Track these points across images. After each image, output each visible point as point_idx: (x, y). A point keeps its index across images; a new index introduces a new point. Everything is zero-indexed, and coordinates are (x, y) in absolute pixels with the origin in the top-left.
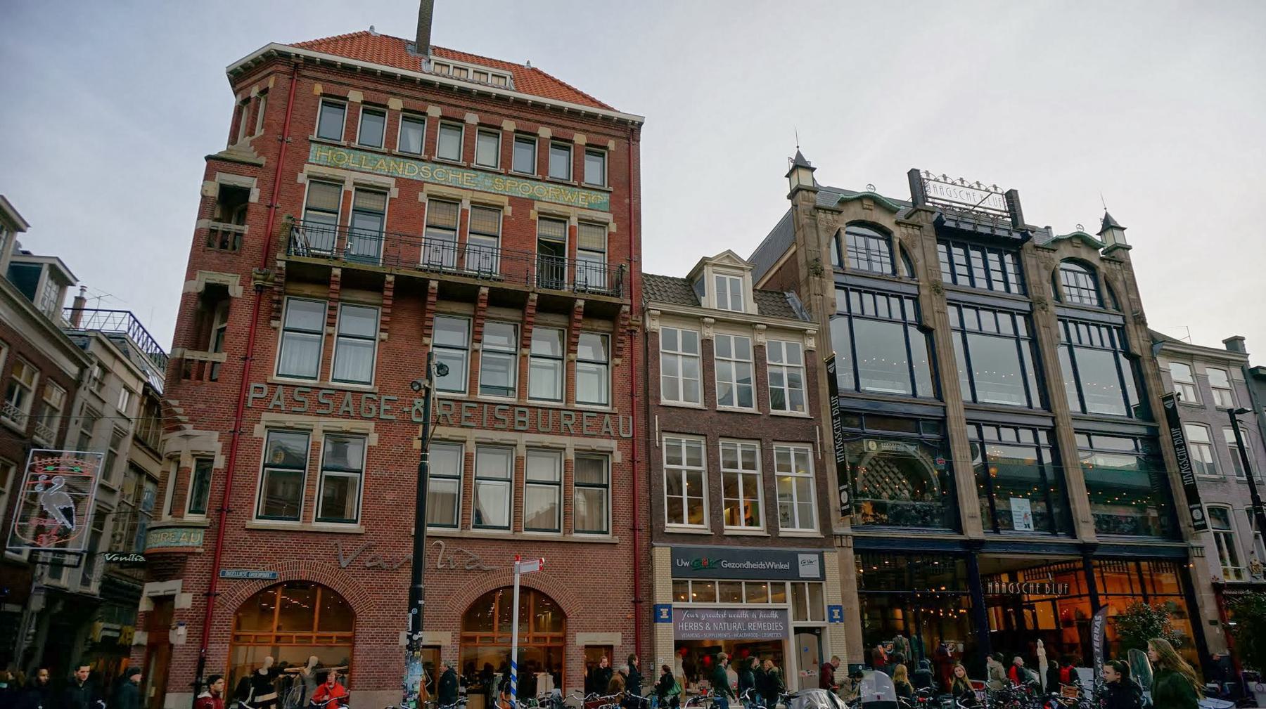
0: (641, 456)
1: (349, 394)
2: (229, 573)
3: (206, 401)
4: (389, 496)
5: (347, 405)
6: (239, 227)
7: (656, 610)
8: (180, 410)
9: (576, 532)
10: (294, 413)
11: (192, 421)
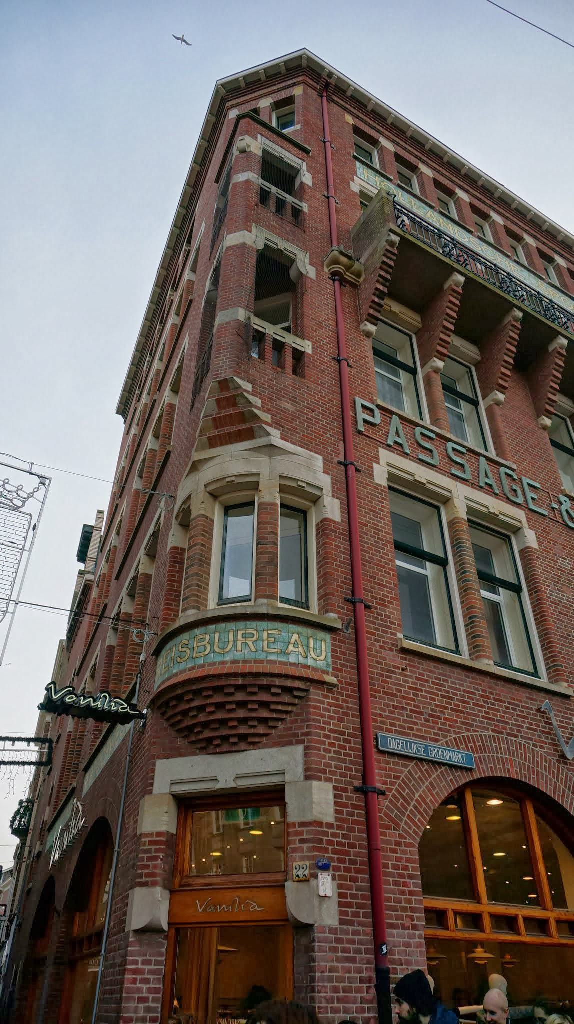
2: (394, 744)
3: (293, 400)
8: (257, 402)
11: (277, 424)
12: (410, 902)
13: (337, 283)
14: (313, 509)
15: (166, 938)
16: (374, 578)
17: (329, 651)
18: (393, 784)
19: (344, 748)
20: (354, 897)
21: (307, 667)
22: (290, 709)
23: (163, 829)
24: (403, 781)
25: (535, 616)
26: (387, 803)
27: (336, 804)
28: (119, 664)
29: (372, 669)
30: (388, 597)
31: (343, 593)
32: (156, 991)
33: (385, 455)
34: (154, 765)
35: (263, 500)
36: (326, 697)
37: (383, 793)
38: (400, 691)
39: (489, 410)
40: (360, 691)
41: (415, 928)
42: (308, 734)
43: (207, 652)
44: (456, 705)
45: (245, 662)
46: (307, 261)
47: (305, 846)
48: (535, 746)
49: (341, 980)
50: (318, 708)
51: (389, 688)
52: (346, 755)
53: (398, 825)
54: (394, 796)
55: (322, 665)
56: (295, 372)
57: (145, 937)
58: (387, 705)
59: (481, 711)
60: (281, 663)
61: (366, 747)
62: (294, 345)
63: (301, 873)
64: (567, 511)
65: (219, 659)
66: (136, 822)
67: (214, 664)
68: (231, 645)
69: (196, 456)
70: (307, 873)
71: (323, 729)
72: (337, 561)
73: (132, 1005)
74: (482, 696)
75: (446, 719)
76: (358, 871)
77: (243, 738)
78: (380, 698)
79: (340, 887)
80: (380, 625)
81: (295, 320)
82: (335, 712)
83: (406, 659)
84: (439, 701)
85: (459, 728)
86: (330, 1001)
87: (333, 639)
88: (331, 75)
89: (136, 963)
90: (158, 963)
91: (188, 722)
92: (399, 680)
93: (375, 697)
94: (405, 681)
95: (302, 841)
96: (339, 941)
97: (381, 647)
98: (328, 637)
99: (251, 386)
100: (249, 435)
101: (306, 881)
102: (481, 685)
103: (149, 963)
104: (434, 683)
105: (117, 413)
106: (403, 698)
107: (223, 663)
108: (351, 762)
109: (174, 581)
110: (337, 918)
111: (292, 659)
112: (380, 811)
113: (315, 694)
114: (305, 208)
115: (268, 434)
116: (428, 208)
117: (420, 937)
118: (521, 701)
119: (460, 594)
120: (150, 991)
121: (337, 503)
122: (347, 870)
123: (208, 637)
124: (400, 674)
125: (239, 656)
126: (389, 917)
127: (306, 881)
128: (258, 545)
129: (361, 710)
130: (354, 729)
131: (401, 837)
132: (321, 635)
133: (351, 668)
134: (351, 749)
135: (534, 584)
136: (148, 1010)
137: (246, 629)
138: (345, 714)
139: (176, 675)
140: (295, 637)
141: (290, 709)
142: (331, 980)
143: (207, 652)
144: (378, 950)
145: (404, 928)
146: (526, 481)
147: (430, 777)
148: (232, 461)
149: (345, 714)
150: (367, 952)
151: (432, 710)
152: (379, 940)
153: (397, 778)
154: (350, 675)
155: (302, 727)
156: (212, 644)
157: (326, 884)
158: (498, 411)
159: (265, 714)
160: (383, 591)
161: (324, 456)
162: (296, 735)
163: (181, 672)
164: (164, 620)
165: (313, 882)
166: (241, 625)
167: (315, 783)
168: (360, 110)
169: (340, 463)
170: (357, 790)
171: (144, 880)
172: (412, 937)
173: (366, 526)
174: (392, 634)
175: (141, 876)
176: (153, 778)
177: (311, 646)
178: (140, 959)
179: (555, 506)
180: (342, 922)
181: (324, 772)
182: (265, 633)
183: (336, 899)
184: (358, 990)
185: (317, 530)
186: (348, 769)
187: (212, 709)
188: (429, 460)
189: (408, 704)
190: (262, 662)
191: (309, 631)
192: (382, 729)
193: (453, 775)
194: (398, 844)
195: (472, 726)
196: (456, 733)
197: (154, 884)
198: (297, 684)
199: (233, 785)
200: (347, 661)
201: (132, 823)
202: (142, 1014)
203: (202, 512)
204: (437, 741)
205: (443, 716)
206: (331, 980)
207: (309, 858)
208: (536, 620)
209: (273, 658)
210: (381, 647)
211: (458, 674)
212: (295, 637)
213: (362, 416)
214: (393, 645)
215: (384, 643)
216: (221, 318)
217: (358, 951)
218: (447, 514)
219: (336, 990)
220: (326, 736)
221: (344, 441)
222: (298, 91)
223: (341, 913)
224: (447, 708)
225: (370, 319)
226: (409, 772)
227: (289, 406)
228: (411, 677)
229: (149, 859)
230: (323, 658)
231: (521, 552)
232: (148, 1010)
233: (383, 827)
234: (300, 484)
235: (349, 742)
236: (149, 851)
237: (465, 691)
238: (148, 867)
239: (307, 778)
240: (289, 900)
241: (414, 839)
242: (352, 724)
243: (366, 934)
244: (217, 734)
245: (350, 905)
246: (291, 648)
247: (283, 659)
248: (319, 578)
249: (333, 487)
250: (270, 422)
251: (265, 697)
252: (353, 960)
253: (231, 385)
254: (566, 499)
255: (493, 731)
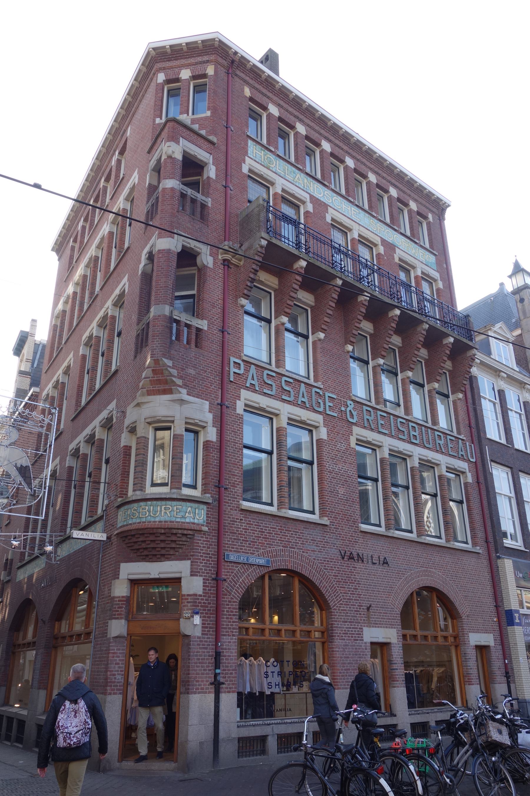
0: (482, 480)
1: (303, 385)
2: (232, 558)
3: (195, 367)
4: (341, 491)
5: (303, 397)
6: (204, 198)
7: (510, 614)
8: (174, 372)
9: (291, 509)
10: (265, 394)
11: (185, 386)
12: (232, 625)
13: (226, 267)
14: (202, 432)
15: (126, 640)
16: (230, 471)
17: (205, 514)
18: (230, 575)
19: (209, 561)
20: (208, 624)
21: (194, 523)
22: (185, 543)
23: (125, 595)
24: (235, 574)
25: (318, 479)
26: (226, 584)
27: (204, 586)
28: (80, 486)
29: (226, 521)
30: (237, 481)
31: (214, 482)
32: (123, 660)
33: (244, 394)
34: (119, 565)
35: (176, 433)
36: (202, 537)
37: (225, 580)
38: (238, 531)
39: (314, 343)
40: (218, 533)
41: (233, 635)
42: (192, 556)
43: (147, 516)
44: (265, 535)
45: (165, 522)
46: (208, 253)
47: (189, 604)
48: (303, 552)
49: (201, 656)
50: (198, 543)
51: (233, 530)
52: (210, 564)
53: (231, 594)
54: (230, 581)
55: (201, 522)
56: (196, 346)
57: (118, 639)
58: (231, 538)
59: (278, 537)
60: (182, 522)
61: (219, 558)
62: (197, 326)
63: (187, 615)
64: (350, 411)
65: (153, 520)
66: (110, 590)
67: (150, 522)
68: (159, 513)
69: (139, 399)
70: (189, 615)
71: (200, 553)
72: (212, 465)
73: (113, 666)
74: (279, 529)
75: (259, 543)
76: (211, 614)
77: (163, 555)
78: (228, 535)
79: (203, 620)
80: (232, 497)
81: (199, 291)
82: (206, 544)
83: (242, 514)
84: (257, 534)
85: (265, 546)
86: (196, 663)
87: (208, 508)
88: (236, 53)
89: (114, 650)
90: (123, 650)
91: (136, 547)
92: (238, 525)
93: (225, 535)
94: (241, 525)
95: (188, 602)
96: (201, 641)
97: (231, 509)
98: (205, 507)
99: (171, 362)
100: (169, 391)
101: (189, 618)
102: (280, 524)
103: (119, 649)
104: (255, 525)
105: (53, 250)
106: (239, 534)
107: (155, 522)
108: (212, 567)
109: (126, 466)
110: (201, 632)
111: (187, 520)
112: (223, 588)
113: (197, 536)
114: (209, 202)
115: (180, 393)
116: (297, 171)
117: (235, 639)
118: (299, 530)
119: (277, 472)
120: (120, 660)
121: (215, 429)
122: (206, 613)
123: (147, 508)
124: (239, 522)
125: (162, 519)
126: (223, 631)
127: (189, 618)
128: (173, 459)
129: (218, 542)
130: (214, 551)
131: (232, 598)
132: (202, 506)
133: (215, 521)
134: (212, 561)
135: (320, 461)
136: (119, 667)
137: (165, 505)
138: (211, 545)
139: (131, 524)
140: (189, 509)
141: (185, 543)
142: (196, 656)
143: (147, 516)
144: (216, 645)
145: (229, 635)
146: (327, 394)
147: (248, 571)
148: (160, 406)
149: (211, 545)
150: (212, 645)
151: (253, 539)
152: (217, 640)
153: (232, 573)
154: (215, 525)
155: (190, 552)
156: (149, 512)
157: (197, 620)
158: (319, 345)
159: (173, 545)
160: (235, 478)
161: (210, 401)
162: (187, 556)
163: (134, 524)
164: (121, 488)
165: (191, 619)
166: (164, 503)
167: (195, 578)
168: (256, 80)
169: (218, 404)
170: (213, 579)
171: (116, 616)
172: (231, 639)
173: (229, 441)
174: (237, 501)
175: (115, 615)
176: (119, 571)
177: (197, 512)
178: (115, 648)
179: (343, 409)
180: (202, 634)
181: (199, 572)
182: (175, 507)
183: (201, 625)
184: (207, 659)
185: (203, 446)
186: (210, 570)
187: (149, 542)
188: (269, 392)
189: (241, 537)
190: (173, 522)
191: (196, 505)
192: (227, 550)
193: (259, 569)
194: (230, 602)
195: (272, 545)
196: (263, 549)
197: (121, 618)
198: (190, 532)
199: (158, 577)
200: (213, 518)
201: (106, 589)
202: (117, 669)
203: (143, 435)
204: (253, 554)
205: (258, 541)
206: (196, 656)
207: (190, 609)
208: (318, 481)
209: (178, 520)
210: (231, 509)
211: (269, 519)
212: (189, 509)
213: (233, 369)
214: (237, 507)
215: (233, 506)
216: (153, 311)
217: (209, 645)
218: (277, 423)
219: (198, 659)
220: (201, 556)
221: (222, 389)
222: (210, 70)
223: (202, 631)
224: (260, 537)
225: (244, 296)
226: (238, 569)
227: (192, 371)
228: (244, 523)
229: (118, 608)
230: (202, 518)
231: (317, 440)
232: (119, 667)
233: (223, 595)
234: (196, 421)
235: (211, 557)
236: (118, 604)
237: (271, 528)
238: (118, 611)
239: (191, 575)
240: (181, 626)
241: (237, 599)
242: (213, 550)
243: (212, 639)
244: (151, 553)
245: (207, 627)
246: (187, 515)
247: (183, 520)
248: (203, 474)
249: (213, 420)
250: (181, 385)
251: (174, 538)
252: (206, 648)
253: (161, 362)
254: (352, 403)
255: (282, 546)
